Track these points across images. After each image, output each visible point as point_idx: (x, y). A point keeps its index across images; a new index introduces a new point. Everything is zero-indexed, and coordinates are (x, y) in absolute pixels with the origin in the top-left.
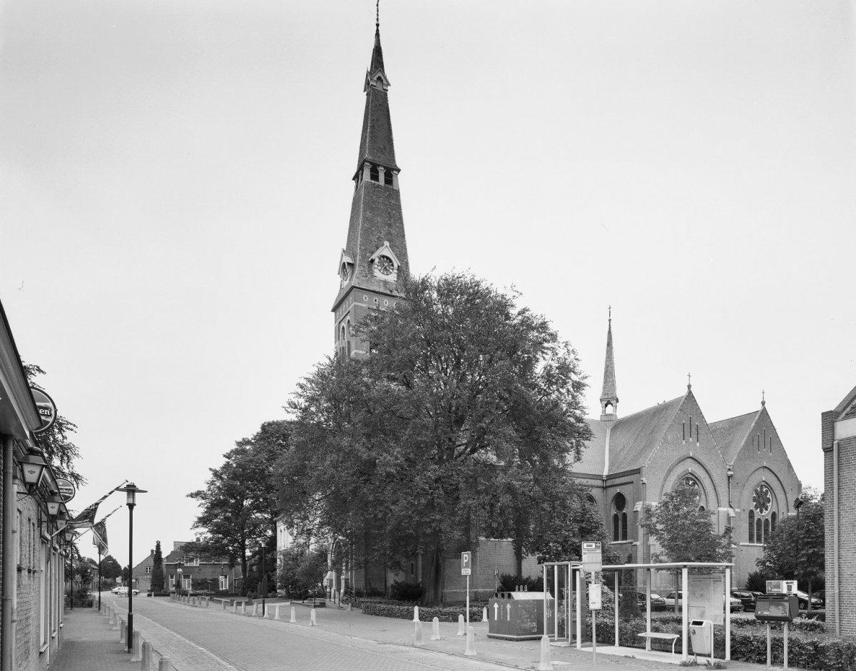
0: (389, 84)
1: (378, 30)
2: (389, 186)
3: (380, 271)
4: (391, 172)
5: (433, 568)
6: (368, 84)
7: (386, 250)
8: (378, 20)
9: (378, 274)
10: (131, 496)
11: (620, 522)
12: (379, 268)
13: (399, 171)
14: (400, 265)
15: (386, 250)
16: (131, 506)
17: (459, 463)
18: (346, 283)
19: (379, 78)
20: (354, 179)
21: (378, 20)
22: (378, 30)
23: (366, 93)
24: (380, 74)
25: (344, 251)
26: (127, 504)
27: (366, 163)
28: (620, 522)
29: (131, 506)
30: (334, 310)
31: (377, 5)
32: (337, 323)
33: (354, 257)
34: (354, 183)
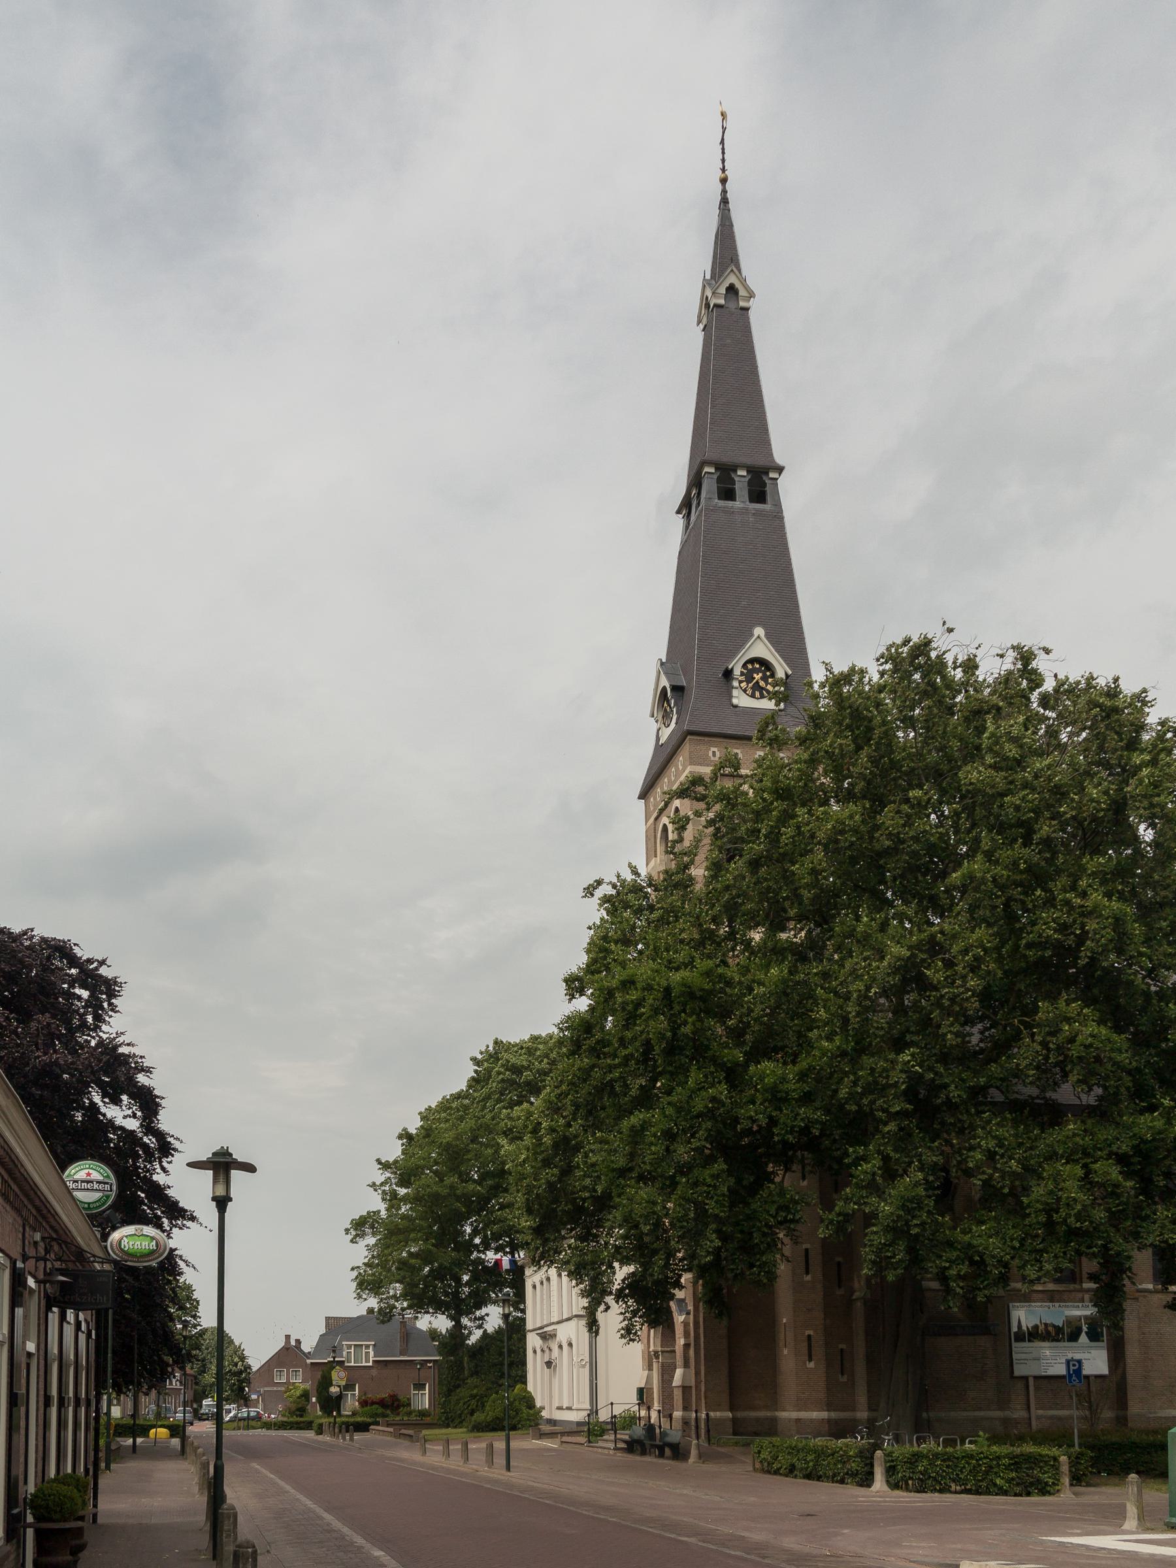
0: (751, 295)
1: (724, 192)
2: (730, 503)
3: (745, 691)
4: (761, 482)
5: (357, 1436)
6: (707, 305)
7: (760, 647)
8: (723, 170)
9: (741, 699)
10: (221, 1178)
11: (54, 1410)
12: (744, 685)
13: (780, 470)
14: (790, 672)
15: (760, 647)
16: (222, 1203)
17: (568, 1101)
18: (666, 733)
19: (732, 289)
20: (678, 512)
21: (723, 170)
22: (724, 192)
23: (701, 326)
24: (732, 279)
25: (662, 664)
26: (214, 1199)
27: (707, 469)
28: (54, 1392)
29: (222, 1203)
30: (643, 795)
31: (722, 142)
32: (652, 820)
33: (686, 672)
34: (679, 521)
